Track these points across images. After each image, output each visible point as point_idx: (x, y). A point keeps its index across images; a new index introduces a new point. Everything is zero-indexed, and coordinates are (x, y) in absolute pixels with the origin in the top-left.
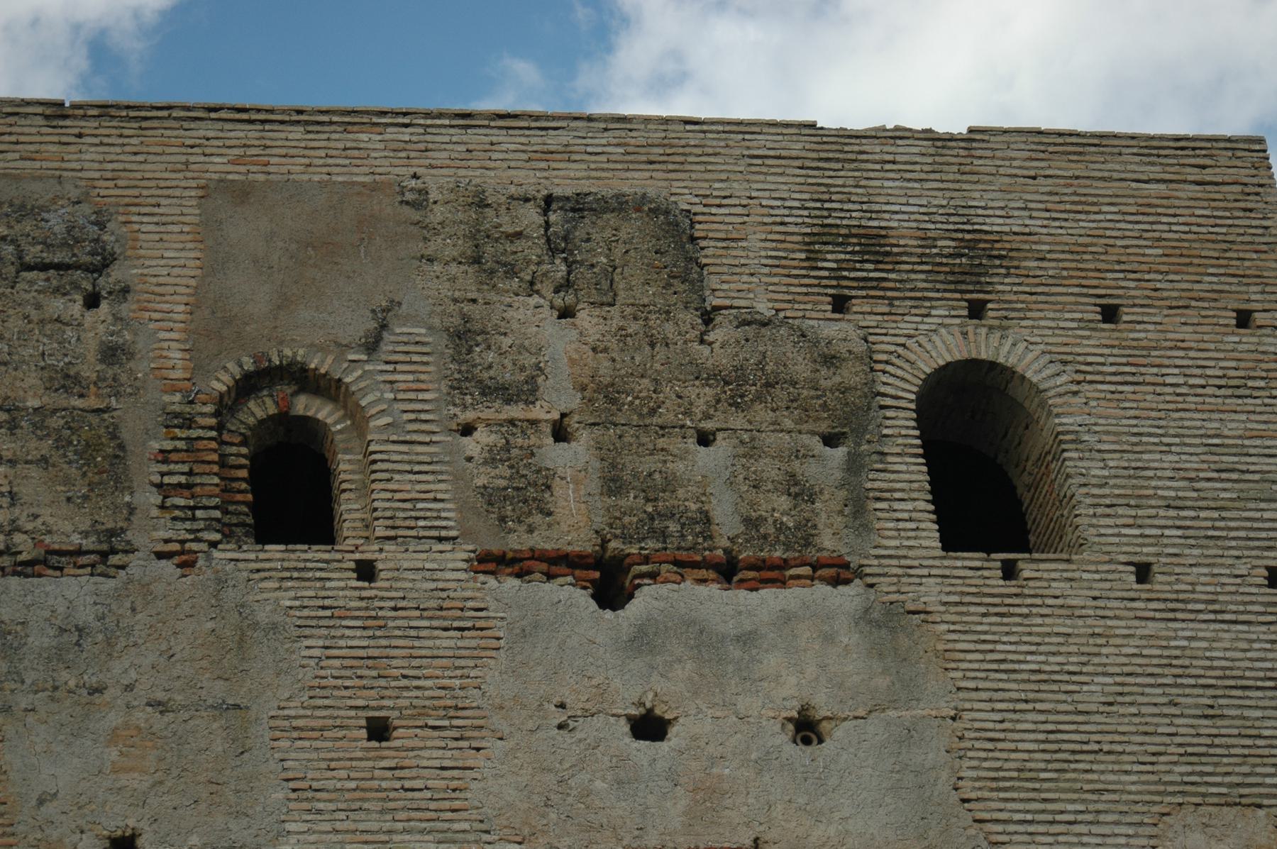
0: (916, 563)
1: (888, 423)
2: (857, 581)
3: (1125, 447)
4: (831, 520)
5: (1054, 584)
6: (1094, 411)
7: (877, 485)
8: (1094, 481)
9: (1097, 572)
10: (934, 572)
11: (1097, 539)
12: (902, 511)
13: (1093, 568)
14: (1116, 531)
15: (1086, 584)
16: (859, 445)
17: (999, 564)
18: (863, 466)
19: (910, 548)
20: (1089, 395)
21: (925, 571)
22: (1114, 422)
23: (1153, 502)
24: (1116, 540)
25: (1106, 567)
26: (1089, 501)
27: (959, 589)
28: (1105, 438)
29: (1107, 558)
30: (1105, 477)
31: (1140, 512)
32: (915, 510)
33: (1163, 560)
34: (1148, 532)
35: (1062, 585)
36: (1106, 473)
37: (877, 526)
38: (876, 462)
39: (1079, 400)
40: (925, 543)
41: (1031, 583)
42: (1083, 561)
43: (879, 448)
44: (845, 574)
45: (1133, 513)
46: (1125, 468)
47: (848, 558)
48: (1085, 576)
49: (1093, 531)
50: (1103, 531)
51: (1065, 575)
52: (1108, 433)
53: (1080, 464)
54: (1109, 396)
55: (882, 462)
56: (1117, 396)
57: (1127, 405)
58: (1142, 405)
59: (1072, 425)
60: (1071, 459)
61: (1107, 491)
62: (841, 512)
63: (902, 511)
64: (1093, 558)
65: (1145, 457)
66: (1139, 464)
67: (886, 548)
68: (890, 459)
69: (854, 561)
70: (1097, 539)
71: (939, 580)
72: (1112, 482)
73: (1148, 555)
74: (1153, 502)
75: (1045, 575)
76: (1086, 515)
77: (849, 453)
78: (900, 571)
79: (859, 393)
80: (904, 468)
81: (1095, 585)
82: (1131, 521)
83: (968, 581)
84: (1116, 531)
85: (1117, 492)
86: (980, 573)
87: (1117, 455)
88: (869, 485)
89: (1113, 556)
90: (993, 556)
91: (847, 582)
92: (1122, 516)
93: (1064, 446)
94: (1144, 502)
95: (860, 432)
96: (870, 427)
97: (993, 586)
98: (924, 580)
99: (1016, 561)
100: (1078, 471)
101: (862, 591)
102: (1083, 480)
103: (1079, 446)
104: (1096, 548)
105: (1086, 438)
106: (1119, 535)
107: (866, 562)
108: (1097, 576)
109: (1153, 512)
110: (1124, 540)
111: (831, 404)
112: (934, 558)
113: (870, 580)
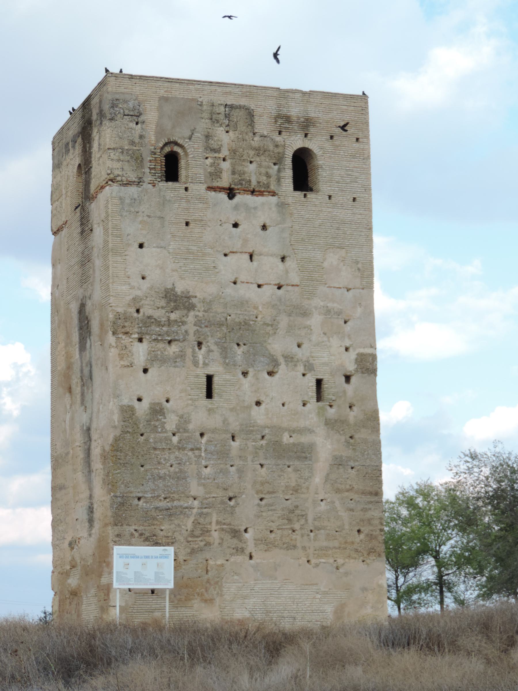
39: (323, 157)
95: (281, 163)
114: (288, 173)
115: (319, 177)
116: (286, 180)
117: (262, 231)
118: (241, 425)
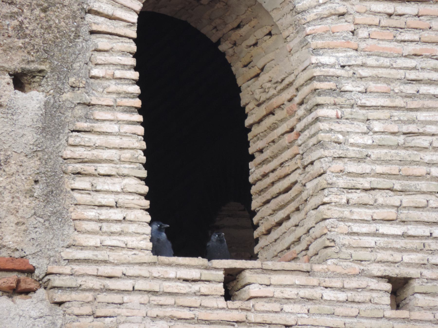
0: (117, 271)
1: (100, 58)
2: (41, 292)
3: (399, 102)
4: (17, 203)
5: (287, 308)
6: (363, 45)
7: (79, 152)
8: (352, 152)
9: (342, 289)
10: (140, 285)
11: (347, 240)
12: (107, 192)
13: (337, 283)
14: (371, 228)
15: (327, 308)
16: (60, 91)
17: (221, 275)
18: (62, 125)
19: (113, 248)
20: (359, 19)
21: (127, 284)
22: (386, 62)
23: (423, 185)
24: (370, 241)
25: (353, 283)
26: (342, 182)
27: (169, 311)
28: (372, 86)
29: (357, 268)
30: (366, 146)
31: (406, 200)
32: (123, 192)
33: (428, 273)
34: (413, 230)
35: (297, 308)
36: (368, 140)
37: (74, 216)
38: (80, 119)
39: (344, 26)
40: (133, 242)
41: (260, 305)
42: (327, 274)
43: (87, 98)
44: (27, 282)
45: (395, 200)
46: (393, 134)
47: (33, 262)
48: (328, 295)
49: (343, 227)
50: (356, 228)
51: (303, 293)
52: (377, 79)
53: (337, 127)
54: (385, 22)
55: (87, 118)
56: (394, 22)
57: (407, 36)
58: (426, 35)
59: (332, 66)
60: (326, 119)
61: (366, 167)
62: (30, 193)
63: (107, 192)
64: (339, 270)
65: (422, 116)
66: (412, 128)
67: (83, 248)
68: (99, 114)
69: (41, 265)
70: (347, 240)
71: (145, 298)
72: (375, 153)
73: (409, 265)
74: (423, 185)
75: (278, 293)
76: (337, 204)
77: (46, 104)
78: (96, 284)
79: (66, 11)
80: (114, 128)
81: (339, 310)
82: (391, 214)
83: (182, 301)
84: (371, 228)
85: (379, 169)
86: (196, 287)
87: (385, 114)
88: (68, 153)
89: (365, 266)
90: (216, 263)
91: (27, 292)
92: (382, 206)
93: (320, 100)
94: (412, 184)
95: (62, 71)
96: (76, 65)
97: (212, 309)
98: (126, 298)
99: (240, 271)
100: (334, 137)
101: (46, 311)
102: (337, 151)
103: (339, 100)
104: (346, 253)
105: (348, 87)
106: (375, 234)
107: (55, 269)
108: (342, 296)
109: (421, 200)
110: (381, 241)
111: (29, 27)
112: (141, 264)
113: (59, 296)
114: (116, 140)
115: (324, 160)
116: (102, 184)
117: (276, 115)
118: (97, 155)
